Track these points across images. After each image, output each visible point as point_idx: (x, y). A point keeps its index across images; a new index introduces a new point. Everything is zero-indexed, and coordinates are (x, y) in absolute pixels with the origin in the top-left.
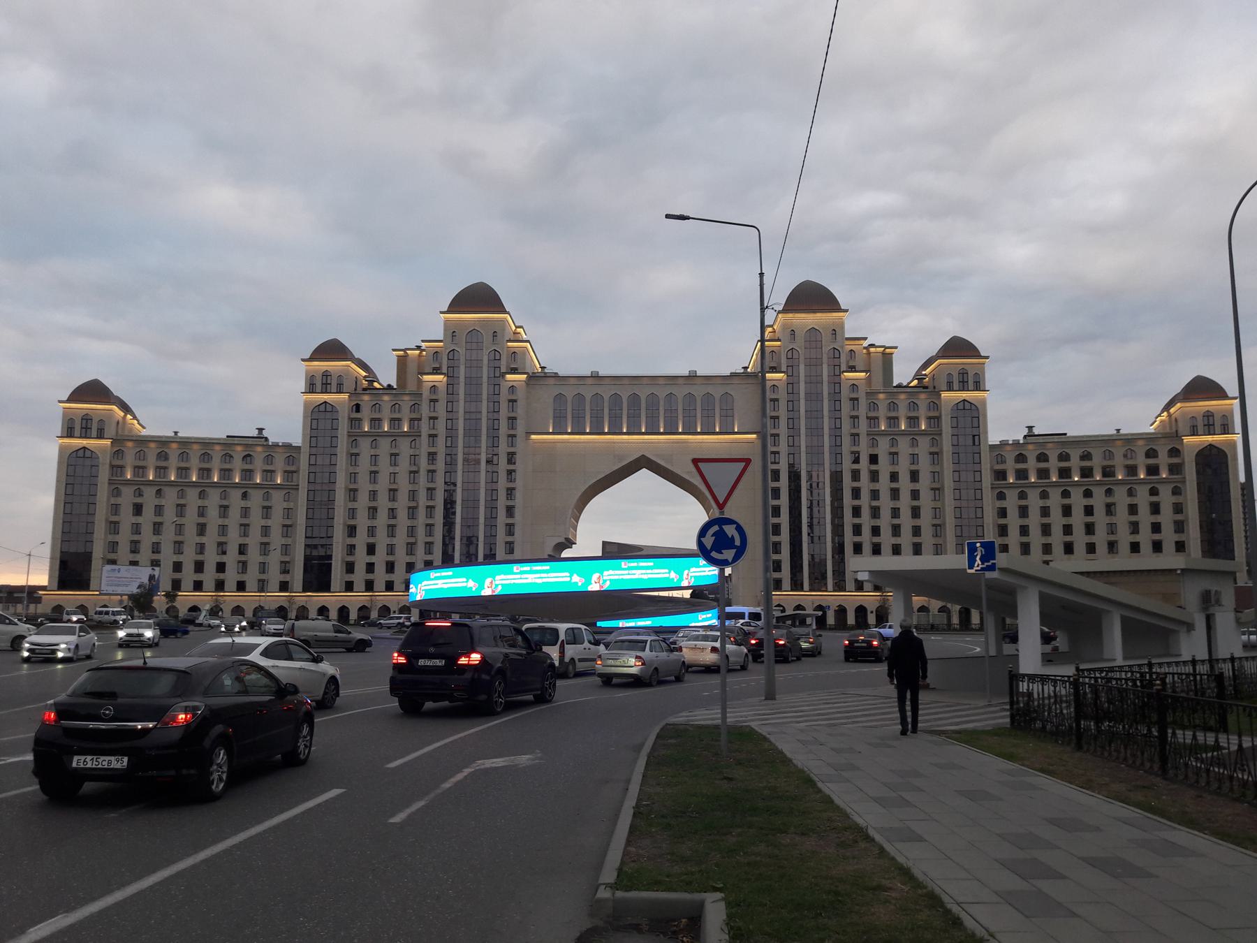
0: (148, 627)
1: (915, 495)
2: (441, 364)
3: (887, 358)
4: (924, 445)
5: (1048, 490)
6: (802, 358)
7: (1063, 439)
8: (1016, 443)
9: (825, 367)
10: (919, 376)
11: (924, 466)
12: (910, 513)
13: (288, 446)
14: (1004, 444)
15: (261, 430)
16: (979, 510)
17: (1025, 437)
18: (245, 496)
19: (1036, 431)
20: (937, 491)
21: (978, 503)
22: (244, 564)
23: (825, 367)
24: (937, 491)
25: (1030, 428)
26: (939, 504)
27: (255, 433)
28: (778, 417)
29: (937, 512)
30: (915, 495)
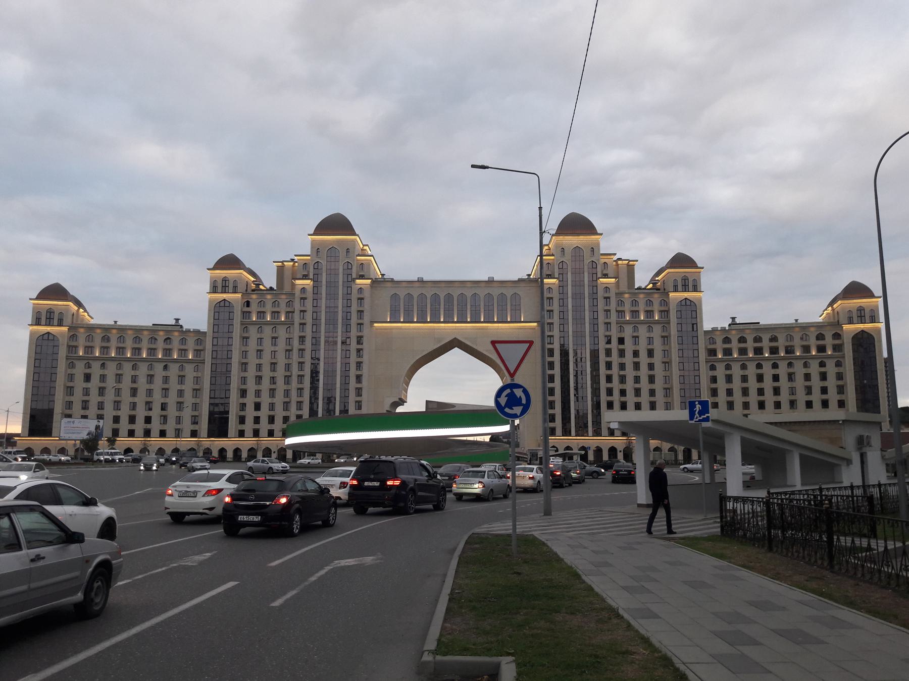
3: (630, 269)
4: (657, 331)
6: (569, 268)
7: (756, 326)
8: (723, 329)
10: (653, 281)
11: (658, 346)
13: (197, 332)
14: (714, 330)
15: (177, 320)
19: (737, 321)
20: (667, 364)
24: (667, 364)
25: (733, 319)
26: (668, 374)
27: (173, 322)
29: (667, 379)
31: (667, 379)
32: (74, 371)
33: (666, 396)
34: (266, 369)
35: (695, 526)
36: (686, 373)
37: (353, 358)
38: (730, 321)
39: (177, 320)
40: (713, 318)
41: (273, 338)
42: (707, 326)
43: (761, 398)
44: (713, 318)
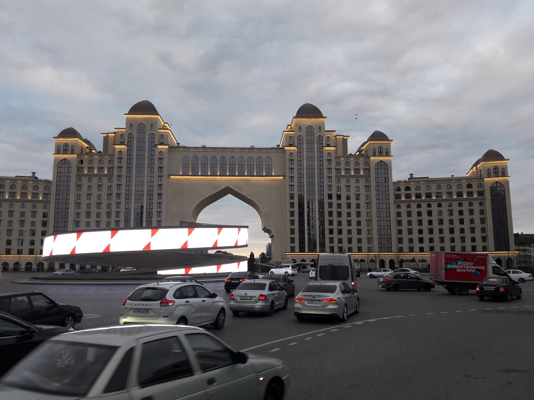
2: (124, 140)
7: (427, 179)
8: (405, 182)
14: (399, 182)
15: (34, 173)
17: (409, 179)
19: (414, 176)
23: (316, 144)
25: (411, 175)
26: (369, 210)
27: (31, 175)
29: (369, 232)
31: (369, 232)
38: (409, 176)
39: (34, 173)
40: (399, 173)
41: (158, 203)
44: (399, 173)
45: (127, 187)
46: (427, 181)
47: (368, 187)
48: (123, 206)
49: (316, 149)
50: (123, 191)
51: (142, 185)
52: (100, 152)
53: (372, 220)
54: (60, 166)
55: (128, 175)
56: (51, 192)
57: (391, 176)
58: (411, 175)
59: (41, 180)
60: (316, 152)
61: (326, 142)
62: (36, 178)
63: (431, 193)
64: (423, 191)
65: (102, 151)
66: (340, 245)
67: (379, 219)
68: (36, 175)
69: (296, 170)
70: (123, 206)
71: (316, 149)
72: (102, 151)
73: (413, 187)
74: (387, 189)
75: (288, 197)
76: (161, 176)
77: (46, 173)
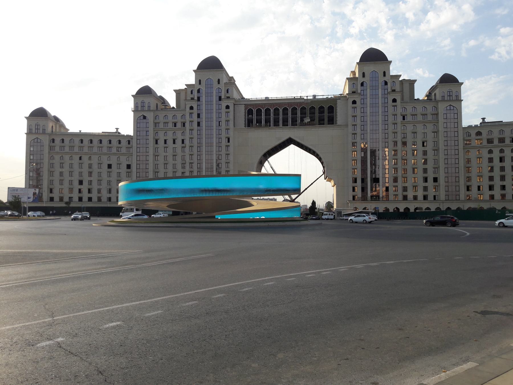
0: (80, 215)
1: (502, 169)
2: (194, 95)
3: (411, 83)
4: (430, 127)
5: (492, 149)
6: (368, 86)
7: (501, 123)
8: (476, 126)
9: (380, 90)
10: (429, 95)
11: (430, 137)
12: (87, 191)
13: (128, 136)
14: (470, 127)
15: (117, 129)
16: (457, 187)
17: (481, 123)
18: (90, 158)
19: (486, 120)
20: (436, 150)
21: (457, 184)
22: (426, 160)
23: (380, 90)
24: (436, 150)
25: (483, 119)
26: (437, 158)
27: (115, 131)
28: (356, 116)
29: (436, 161)
30: (502, 169)
31: (436, 161)
32: (54, 161)
33: (434, 173)
34: (170, 159)
35: (91, 270)
36: (449, 130)
37: (224, 152)
38: (481, 121)
39: (117, 129)
40: (471, 116)
41: (226, 163)
42: (465, 123)
43: (503, 173)
44: (471, 116)
45: (199, 156)
46: (499, 124)
47: (436, 132)
48: (195, 157)
49: (380, 96)
50: (195, 141)
51: (212, 146)
52: (173, 108)
53: (439, 167)
54: (139, 121)
55: (199, 153)
56: (132, 146)
57: (461, 121)
58: (483, 119)
59: (124, 136)
60: (380, 98)
61: (391, 87)
62: (119, 133)
63: (504, 138)
64: (496, 135)
65: (175, 107)
66: (405, 193)
67: (447, 175)
68: (119, 131)
69: (358, 119)
70: (195, 157)
71: (380, 96)
72: (175, 107)
73: (485, 132)
74: (457, 162)
75: (351, 180)
76: (228, 154)
77: (128, 129)
